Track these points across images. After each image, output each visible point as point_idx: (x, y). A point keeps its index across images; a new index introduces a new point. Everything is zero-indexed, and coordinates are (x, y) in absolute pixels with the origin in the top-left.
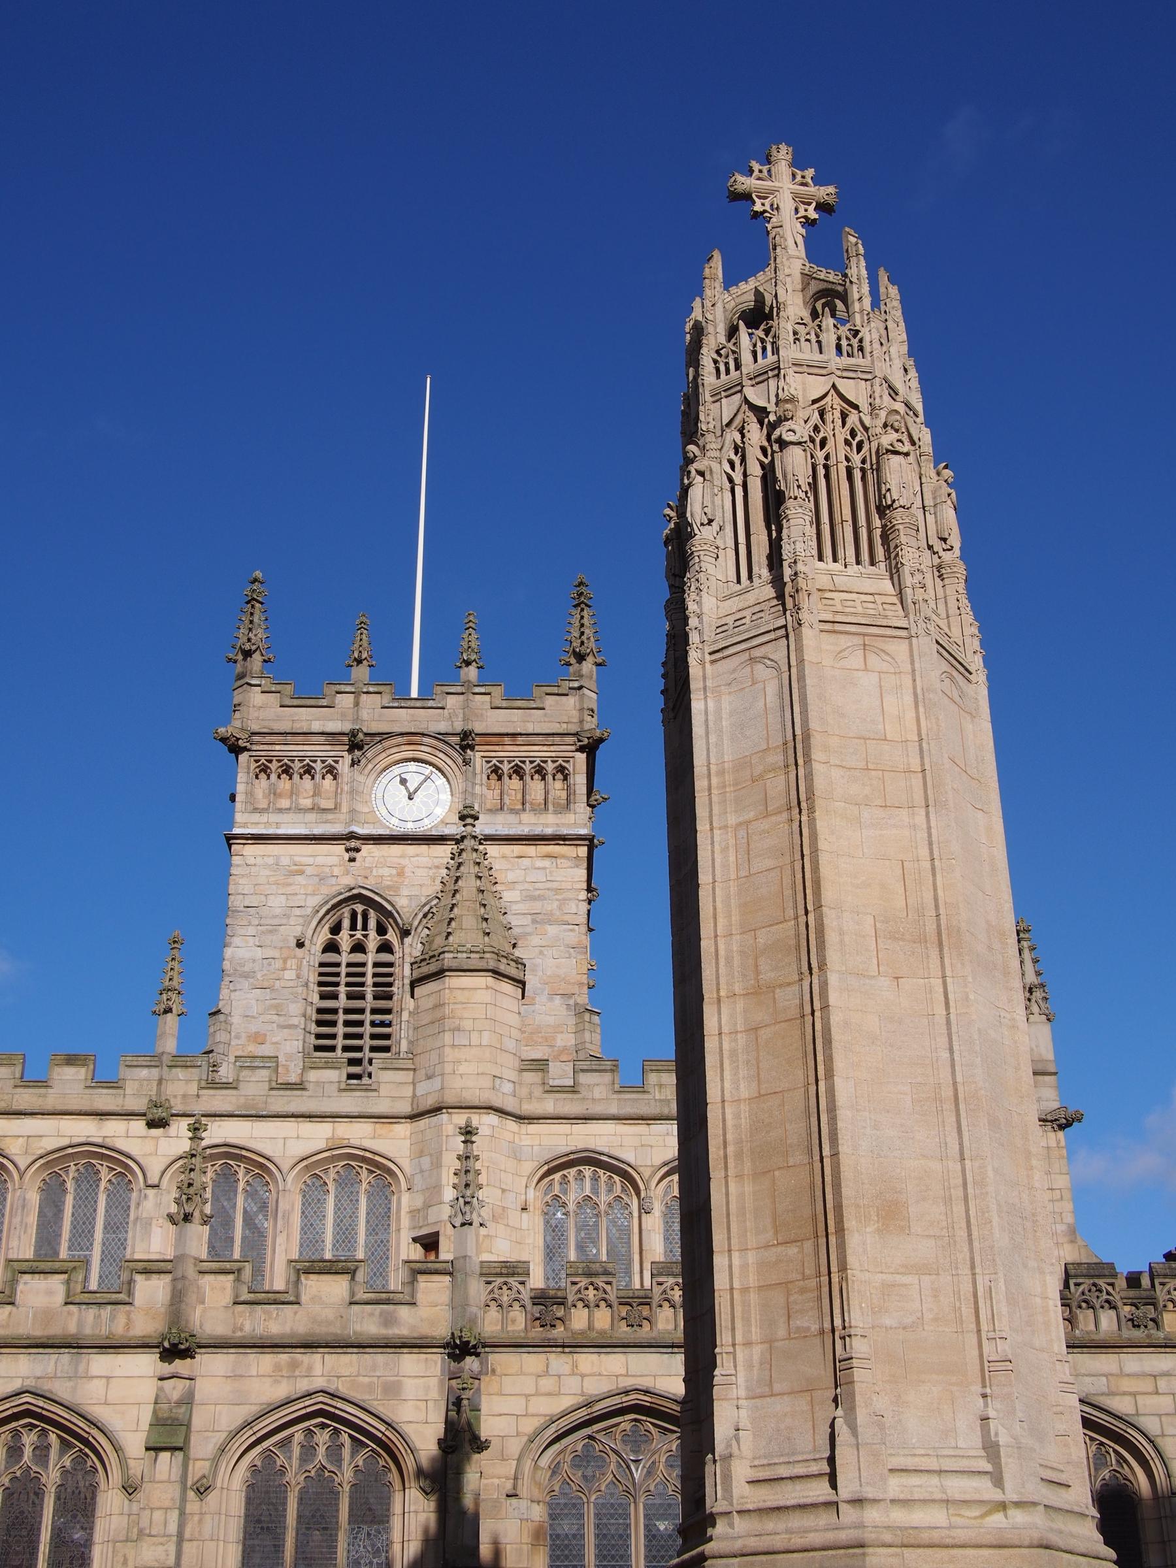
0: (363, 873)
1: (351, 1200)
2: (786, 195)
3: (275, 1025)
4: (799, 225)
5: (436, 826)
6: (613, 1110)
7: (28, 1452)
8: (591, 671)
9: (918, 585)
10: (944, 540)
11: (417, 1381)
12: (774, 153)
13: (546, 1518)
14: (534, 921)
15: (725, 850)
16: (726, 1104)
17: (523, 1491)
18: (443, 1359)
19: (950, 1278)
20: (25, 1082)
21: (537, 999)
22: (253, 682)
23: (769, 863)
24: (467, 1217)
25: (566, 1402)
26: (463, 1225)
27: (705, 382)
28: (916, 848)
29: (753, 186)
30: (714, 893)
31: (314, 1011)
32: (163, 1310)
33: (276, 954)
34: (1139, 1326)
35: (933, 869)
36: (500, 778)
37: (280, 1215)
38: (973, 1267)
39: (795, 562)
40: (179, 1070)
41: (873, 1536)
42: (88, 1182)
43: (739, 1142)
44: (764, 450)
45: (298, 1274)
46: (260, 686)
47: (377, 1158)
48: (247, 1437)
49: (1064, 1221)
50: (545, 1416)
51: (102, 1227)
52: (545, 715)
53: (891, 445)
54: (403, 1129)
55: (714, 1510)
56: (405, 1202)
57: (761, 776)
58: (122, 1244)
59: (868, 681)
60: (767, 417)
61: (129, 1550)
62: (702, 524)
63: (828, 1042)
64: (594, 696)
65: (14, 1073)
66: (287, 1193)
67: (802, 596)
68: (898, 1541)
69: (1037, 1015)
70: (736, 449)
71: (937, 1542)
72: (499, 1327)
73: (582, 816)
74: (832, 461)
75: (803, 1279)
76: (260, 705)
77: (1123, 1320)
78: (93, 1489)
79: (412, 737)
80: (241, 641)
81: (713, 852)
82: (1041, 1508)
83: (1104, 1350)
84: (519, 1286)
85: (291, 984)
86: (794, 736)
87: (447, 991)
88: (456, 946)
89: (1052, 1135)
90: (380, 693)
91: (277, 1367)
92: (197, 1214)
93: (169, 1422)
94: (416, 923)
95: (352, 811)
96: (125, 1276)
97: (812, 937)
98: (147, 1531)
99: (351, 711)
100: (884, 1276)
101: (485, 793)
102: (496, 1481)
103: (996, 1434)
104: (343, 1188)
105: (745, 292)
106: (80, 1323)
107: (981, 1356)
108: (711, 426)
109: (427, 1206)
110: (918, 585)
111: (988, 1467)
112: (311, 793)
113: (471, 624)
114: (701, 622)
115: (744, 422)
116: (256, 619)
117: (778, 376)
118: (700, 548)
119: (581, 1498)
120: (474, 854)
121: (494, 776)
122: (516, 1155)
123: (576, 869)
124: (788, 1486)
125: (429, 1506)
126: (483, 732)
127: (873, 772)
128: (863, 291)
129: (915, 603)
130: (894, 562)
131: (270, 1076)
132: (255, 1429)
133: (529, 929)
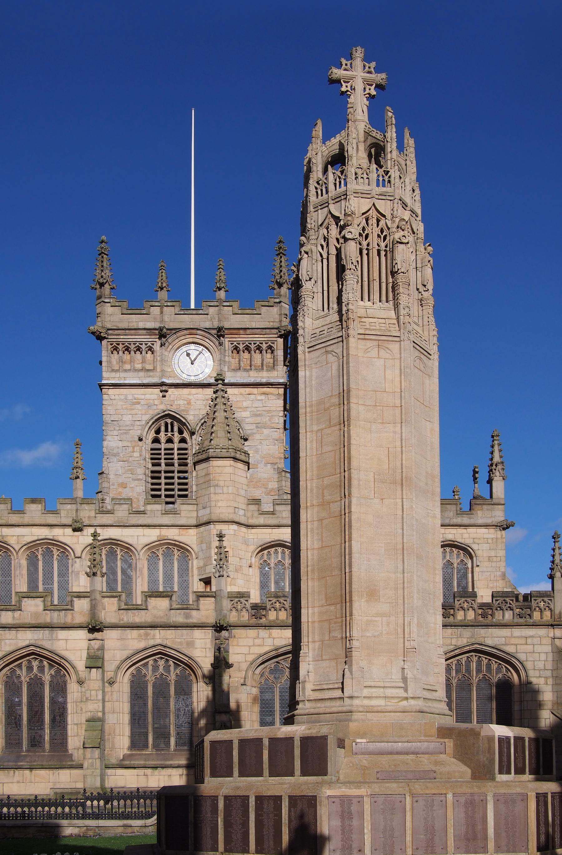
0: (169, 403)
1: (170, 563)
2: (359, 80)
3: (131, 479)
4: (365, 99)
5: (206, 378)
7: (35, 668)
8: (286, 293)
9: (406, 314)
10: (425, 286)
11: (202, 640)
12: (354, 53)
13: (258, 693)
14: (257, 427)
15: (311, 441)
16: (308, 550)
17: (248, 682)
18: (212, 632)
19: (394, 618)
20: (13, 511)
21: (259, 465)
22: (106, 300)
23: (330, 448)
24: (221, 573)
25: (267, 649)
26: (219, 576)
27: (311, 200)
28: (395, 442)
29: (341, 75)
30: (306, 461)
31: (150, 472)
32: (87, 612)
33: (129, 444)
34: (522, 617)
35: (402, 451)
36: (238, 352)
37: (138, 570)
38: (404, 614)
39: (348, 304)
40: (85, 505)
41: (356, 709)
42: (48, 555)
43: (313, 565)
44: (338, 240)
45: (146, 598)
46: (109, 303)
47: (181, 544)
48: (129, 663)
49: (501, 571)
50: (257, 654)
51: (57, 575)
52: (262, 318)
53: (399, 238)
54: (193, 531)
55: (299, 700)
56: (195, 564)
57: (328, 408)
58: (67, 582)
59: (379, 363)
60: (340, 222)
61: (83, 705)
62: (306, 281)
63: (350, 526)
64: (287, 306)
65: (7, 507)
66: (140, 560)
67: (351, 321)
68: (365, 711)
69: (498, 477)
70: (325, 238)
71: (380, 711)
72: (237, 619)
73: (281, 372)
74: (370, 247)
75: (336, 619)
76: (111, 313)
77: (515, 615)
78: (65, 683)
79: (192, 330)
80: (98, 277)
81: (306, 443)
82: (422, 699)
83: (505, 627)
84: (245, 602)
85: (137, 459)
86: (343, 390)
87: (211, 467)
88: (215, 446)
89: (499, 532)
90: (174, 306)
91: (140, 635)
92: (99, 573)
93: (95, 657)
94: (198, 428)
95: (162, 371)
96: (69, 599)
97: (346, 482)
98: (90, 698)
99: (159, 316)
100: (368, 618)
101: (232, 360)
102: (237, 679)
103: (407, 674)
104: (166, 558)
105: (333, 144)
106: (51, 618)
107: (404, 646)
108: (313, 225)
109: (205, 565)
110: (406, 314)
111: (403, 685)
112: (141, 361)
113: (221, 266)
114: (304, 332)
115: (329, 225)
116: (105, 265)
117: (346, 198)
118: (305, 294)
119: (273, 686)
120: (223, 399)
121: (235, 351)
122: (246, 542)
123: (278, 400)
124: (327, 692)
125: (208, 689)
126: (229, 327)
127: (378, 407)
128: (393, 147)
129: (404, 324)
130: (396, 302)
131: (129, 508)
132: (132, 660)
133: (254, 431)
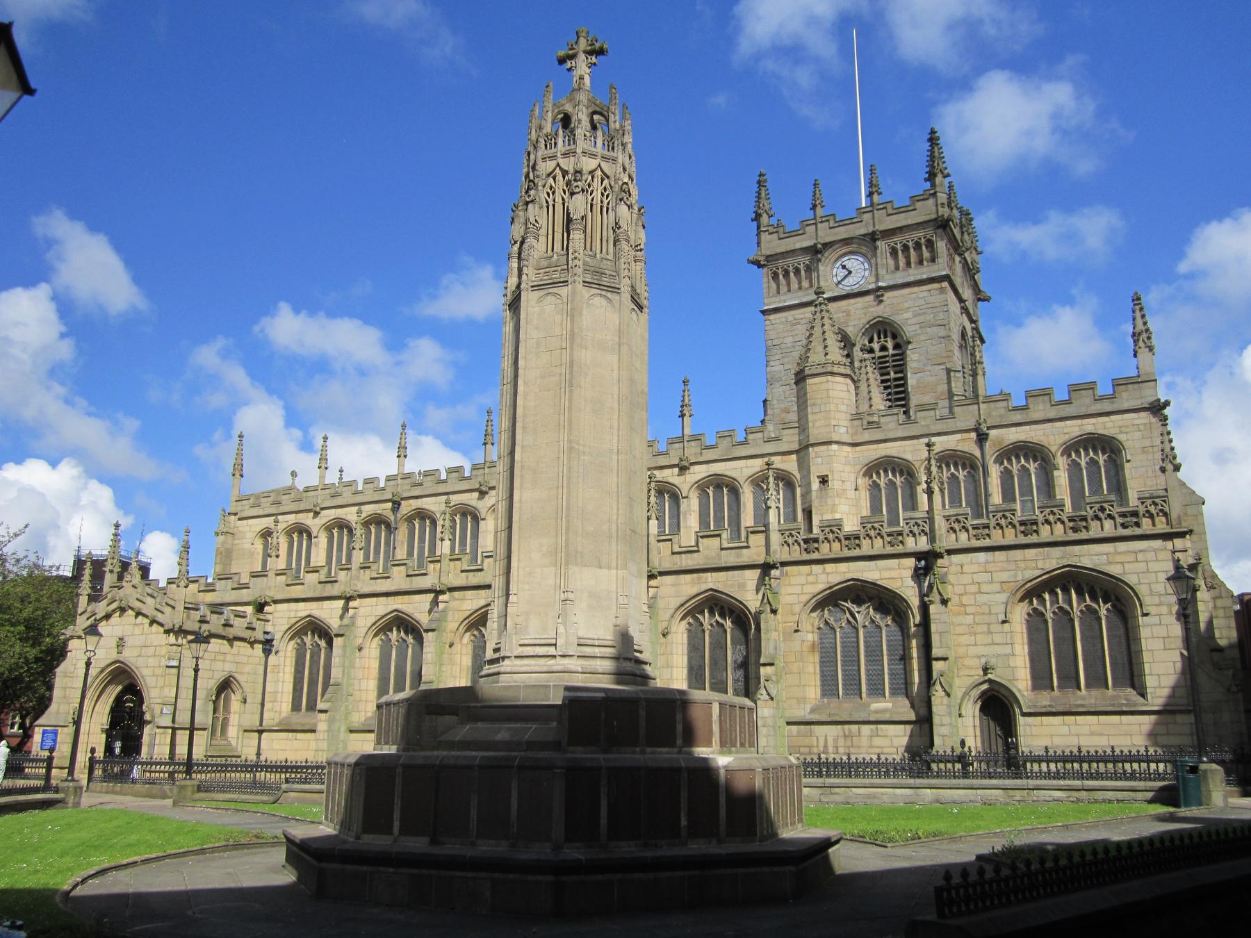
6: (900, 435)
14: (921, 327)
25: (821, 587)
79: (846, 241)
133: (919, 332)
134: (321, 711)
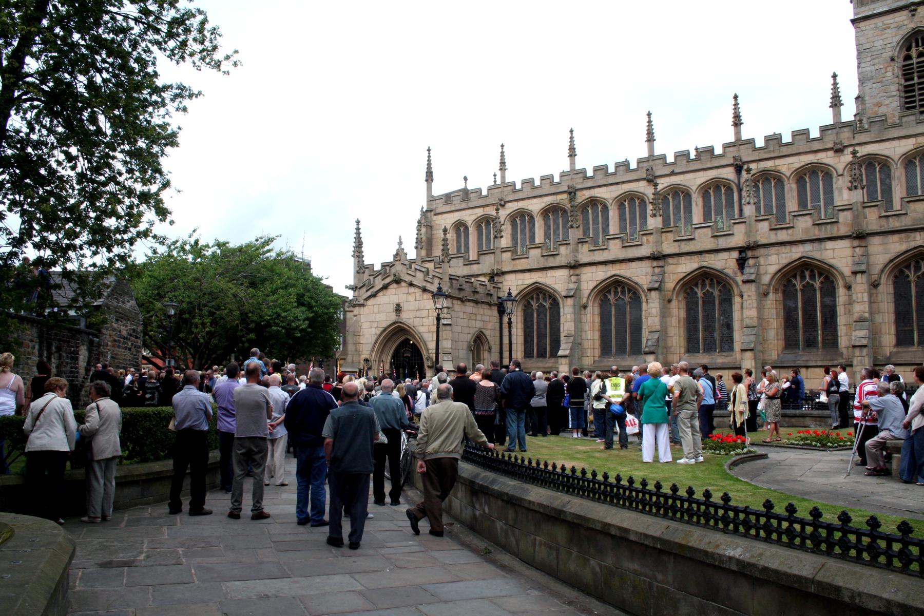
134: (646, 353)
